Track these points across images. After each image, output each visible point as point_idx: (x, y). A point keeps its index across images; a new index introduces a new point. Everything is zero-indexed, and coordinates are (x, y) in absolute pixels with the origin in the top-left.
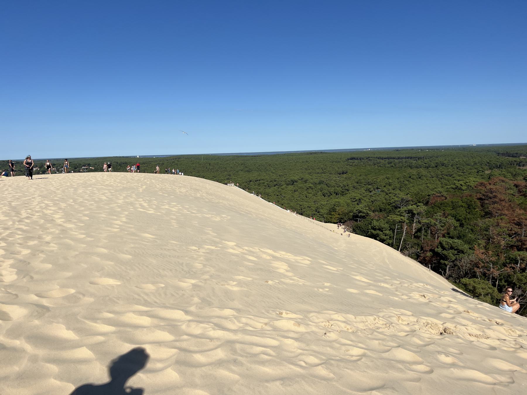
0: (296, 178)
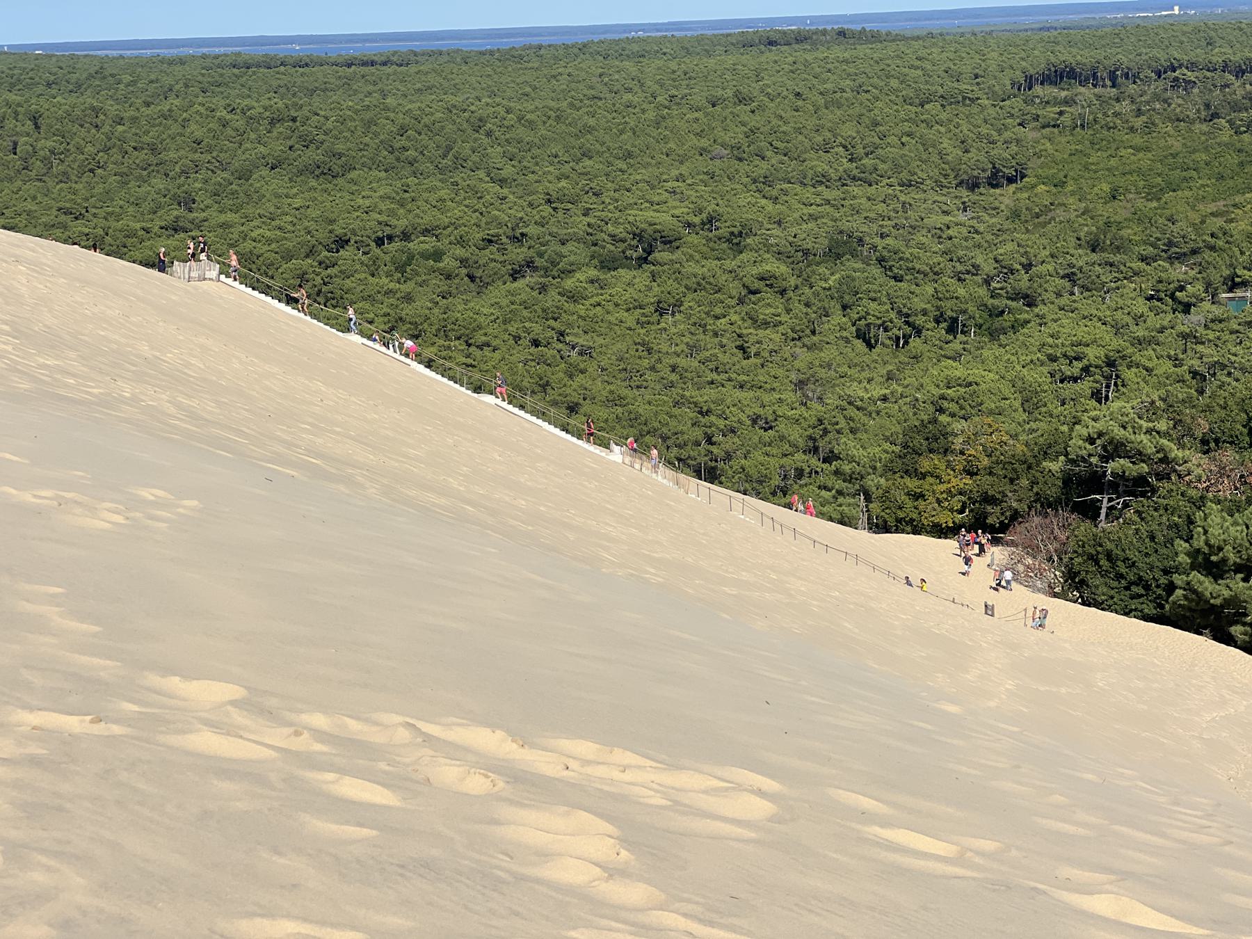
0: (664, 219)
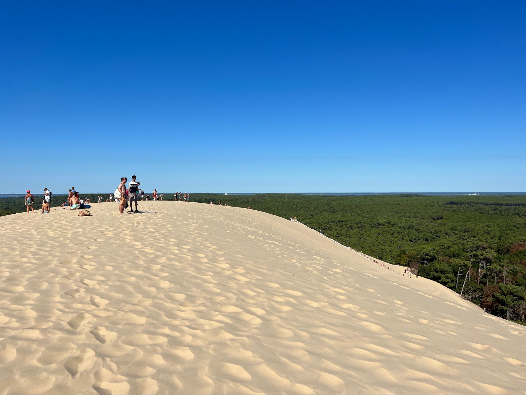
0: (382, 221)
